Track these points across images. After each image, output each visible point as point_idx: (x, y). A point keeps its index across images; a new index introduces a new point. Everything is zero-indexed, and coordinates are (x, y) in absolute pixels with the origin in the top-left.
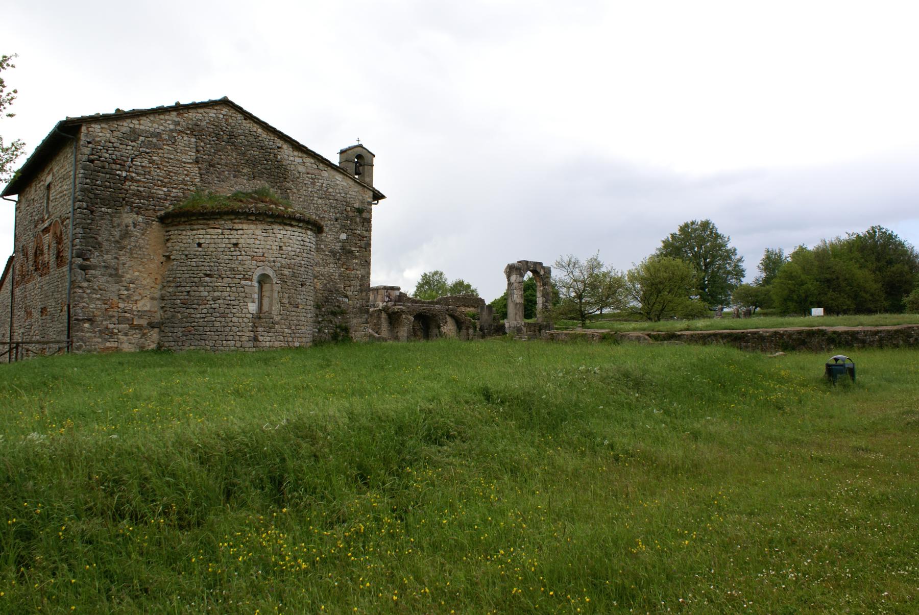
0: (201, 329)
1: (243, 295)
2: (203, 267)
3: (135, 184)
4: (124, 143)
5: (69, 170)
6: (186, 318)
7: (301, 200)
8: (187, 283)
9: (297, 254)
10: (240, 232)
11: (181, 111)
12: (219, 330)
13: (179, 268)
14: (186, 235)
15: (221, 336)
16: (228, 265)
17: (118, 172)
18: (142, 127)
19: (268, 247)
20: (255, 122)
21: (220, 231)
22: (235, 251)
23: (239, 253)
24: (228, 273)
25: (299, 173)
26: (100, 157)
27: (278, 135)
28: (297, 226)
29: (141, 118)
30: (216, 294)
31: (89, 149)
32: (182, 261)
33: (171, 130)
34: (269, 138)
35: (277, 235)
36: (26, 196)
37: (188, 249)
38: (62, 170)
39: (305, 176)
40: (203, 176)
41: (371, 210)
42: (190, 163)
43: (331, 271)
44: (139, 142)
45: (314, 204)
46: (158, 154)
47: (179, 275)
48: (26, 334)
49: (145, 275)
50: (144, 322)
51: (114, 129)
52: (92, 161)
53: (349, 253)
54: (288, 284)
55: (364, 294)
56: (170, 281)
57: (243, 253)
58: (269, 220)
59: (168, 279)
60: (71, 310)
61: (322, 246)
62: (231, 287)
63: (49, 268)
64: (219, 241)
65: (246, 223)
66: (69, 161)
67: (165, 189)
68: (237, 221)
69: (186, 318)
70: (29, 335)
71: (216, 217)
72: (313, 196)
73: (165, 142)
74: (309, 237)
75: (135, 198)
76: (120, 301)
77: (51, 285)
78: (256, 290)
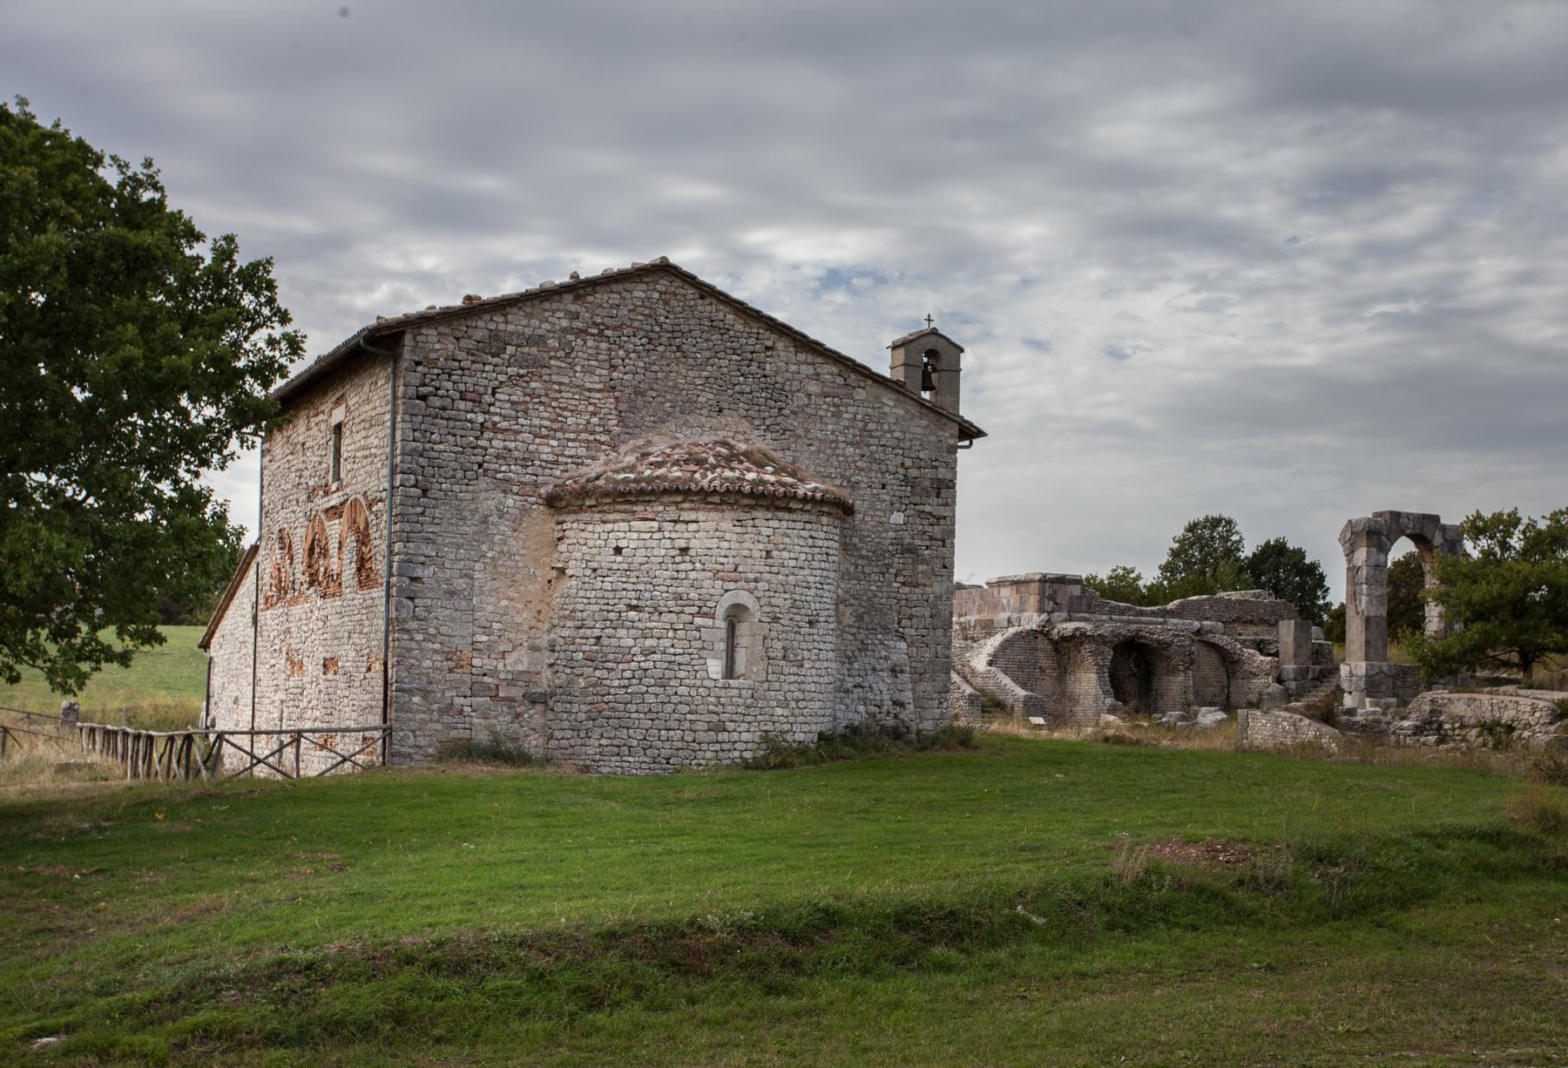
0: (621, 707)
1: (698, 644)
2: (624, 593)
3: (500, 436)
4: (479, 359)
5: (379, 410)
6: (594, 686)
7: (813, 448)
8: (596, 621)
9: (800, 563)
10: (692, 527)
11: (581, 292)
12: (653, 710)
13: (581, 593)
14: (594, 532)
15: (656, 721)
16: (671, 589)
17: (469, 416)
18: (511, 328)
19: (746, 553)
20: (723, 302)
21: (655, 524)
22: (684, 562)
23: (690, 566)
24: (671, 603)
25: (809, 395)
26: (438, 389)
27: (766, 324)
28: (801, 510)
29: (508, 310)
30: (649, 643)
31: (418, 375)
32: (587, 579)
33: (564, 331)
34: (747, 330)
35: (762, 529)
36: (285, 433)
37: (598, 558)
38: (367, 407)
39: (820, 401)
40: (623, 414)
41: (955, 461)
42: (600, 391)
43: (873, 588)
44: (507, 357)
45: (838, 455)
46: (541, 377)
47: (580, 607)
48: (291, 703)
49: (520, 606)
50: (516, 693)
51: (461, 335)
52: (424, 398)
53: (910, 551)
54: (782, 621)
55: (940, 632)
56: (565, 617)
57: (698, 565)
58: (746, 502)
59: (562, 613)
60: (390, 671)
61: (855, 540)
62: (676, 630)
63: (340, 584)
64: (655, 543)
65: (704, 509)
66: (382, 394)
67: (554, 443)
68: (686, 505)
69: (594, 686)
70: (298, 707)
71: (647, 498)
72: (837, 441)
73: (552, 354)
74: (825, 528)
75: (500, 462)
76: (475, 654)
77: (346, 619)
78: (723, 634)
